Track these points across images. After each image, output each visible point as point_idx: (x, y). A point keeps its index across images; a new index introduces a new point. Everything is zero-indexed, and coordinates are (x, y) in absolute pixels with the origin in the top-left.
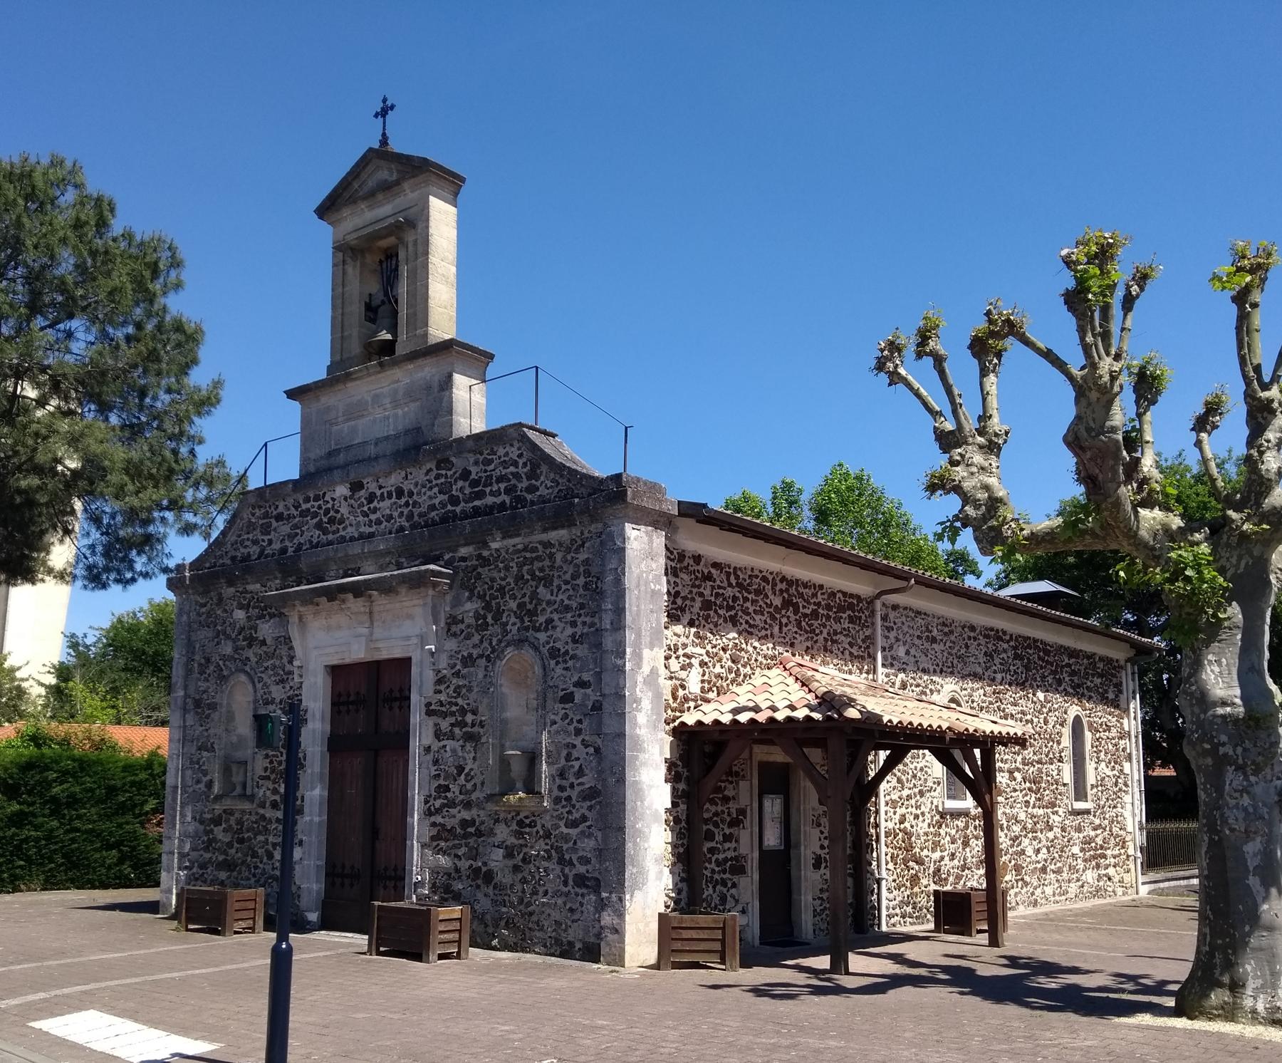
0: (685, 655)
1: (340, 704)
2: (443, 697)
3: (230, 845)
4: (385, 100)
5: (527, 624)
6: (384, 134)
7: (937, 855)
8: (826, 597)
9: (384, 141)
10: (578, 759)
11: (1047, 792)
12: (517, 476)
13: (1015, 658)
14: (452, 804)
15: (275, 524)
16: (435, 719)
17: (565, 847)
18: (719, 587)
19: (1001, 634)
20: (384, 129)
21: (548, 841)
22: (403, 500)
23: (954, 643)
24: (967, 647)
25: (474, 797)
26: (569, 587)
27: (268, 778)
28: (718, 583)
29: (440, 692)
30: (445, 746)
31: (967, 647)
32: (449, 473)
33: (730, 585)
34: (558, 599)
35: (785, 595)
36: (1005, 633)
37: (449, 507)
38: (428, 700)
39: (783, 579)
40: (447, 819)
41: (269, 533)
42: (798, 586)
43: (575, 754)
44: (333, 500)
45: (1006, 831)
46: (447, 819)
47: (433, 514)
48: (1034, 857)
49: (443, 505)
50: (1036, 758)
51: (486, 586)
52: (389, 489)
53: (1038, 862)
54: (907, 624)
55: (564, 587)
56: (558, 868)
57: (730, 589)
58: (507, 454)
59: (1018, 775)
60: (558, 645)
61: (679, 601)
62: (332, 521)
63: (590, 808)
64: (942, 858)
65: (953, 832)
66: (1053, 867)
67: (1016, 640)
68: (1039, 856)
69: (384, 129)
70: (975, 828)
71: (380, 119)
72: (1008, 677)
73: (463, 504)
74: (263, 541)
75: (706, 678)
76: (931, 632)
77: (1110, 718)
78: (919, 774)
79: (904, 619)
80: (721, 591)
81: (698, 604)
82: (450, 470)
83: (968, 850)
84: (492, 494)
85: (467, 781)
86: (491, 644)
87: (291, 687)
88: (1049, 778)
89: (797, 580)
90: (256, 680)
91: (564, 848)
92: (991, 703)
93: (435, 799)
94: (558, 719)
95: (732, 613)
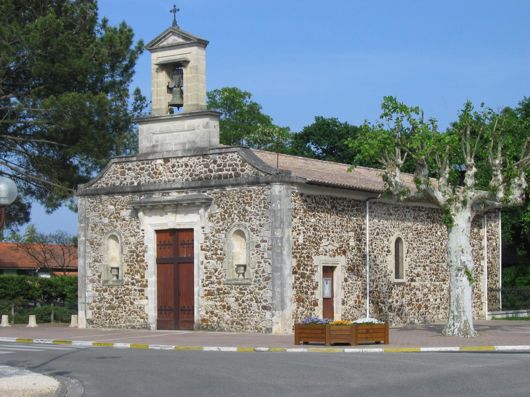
0: (299, 230)
1: (160, 245)
2: (208, 244)
3: (112, 300)
4: (175, 6)
5: (242, 219)
6: (175, 20)
7: (390, 301)
8: (347, 202)
9: (175, 23)
10: (262, 267)
11: (441, 275)
12: (236, 164)
13: (427, 218)
14: (212, 283)
15: (127, 172)
16: (204, 252)
17: (258, 297)
18: (309, 204)
19: (421, 208)
20: (175, 17)
21: (251, 295)
22: (188, 168)
23: (399, 215)
24: (405, 215)
25: (222, 280)
26: (258, 207)
27: (129, 274)
28: (309, 202)
29: (206, 242)
30: (209, 262)
31: (405, 215)
32: (208, 161)
33: (313, 203)
34: (254, 211)
35: (332, 204)
36: (423, 208)
37: (208, 173)
38: (201, 245)
39: (332, 198)
40: (211, 288)
41: (125, 175)
42: (337, 199)
43: (261, 265)
44: (156, 165)
45: (421, 291)
46: (211, 288)
47: (202, 175)
48: (434, 303)
49: (206, 172)
50: (436, 260)
51: (224, 204)
52: (181, 163)
53: (435, 304)
54: (379, 209)
55: (256, 207)
56: (256, 304)
57: (313, 204)
58: (232, 156)
59: (427, 268)
60: (254, 227)
61: (296, 211)
62: (155, 173)
63: (267, 283)
64: (393, 302)
65: (398, 292)
66: (443, 307)
67: (428, 210)
68: (437, 302)
69: (175, 17)
70: (407, 290)
71: (173, 14)
72: (424, 227)
73: (214, 173)
74: (122, 178)
75: (305, 237)
76: (390, 211)
77: (475, 240)
78: (383, 269)
79: (378, 207)
80: (310, 205)
81: (302, 211)
82: (208, 159)
83: (404, 299)
84: (226, 170)
85: (219, 275)
86: (227, 225)
87: (138, 238)
88: (442, 269)
89: (337, 198)
90: (121, 235)
91: (258, 297)
92: (415, 238)
93: (206, 281)
94: (254, 253)
95: (314, 213)
